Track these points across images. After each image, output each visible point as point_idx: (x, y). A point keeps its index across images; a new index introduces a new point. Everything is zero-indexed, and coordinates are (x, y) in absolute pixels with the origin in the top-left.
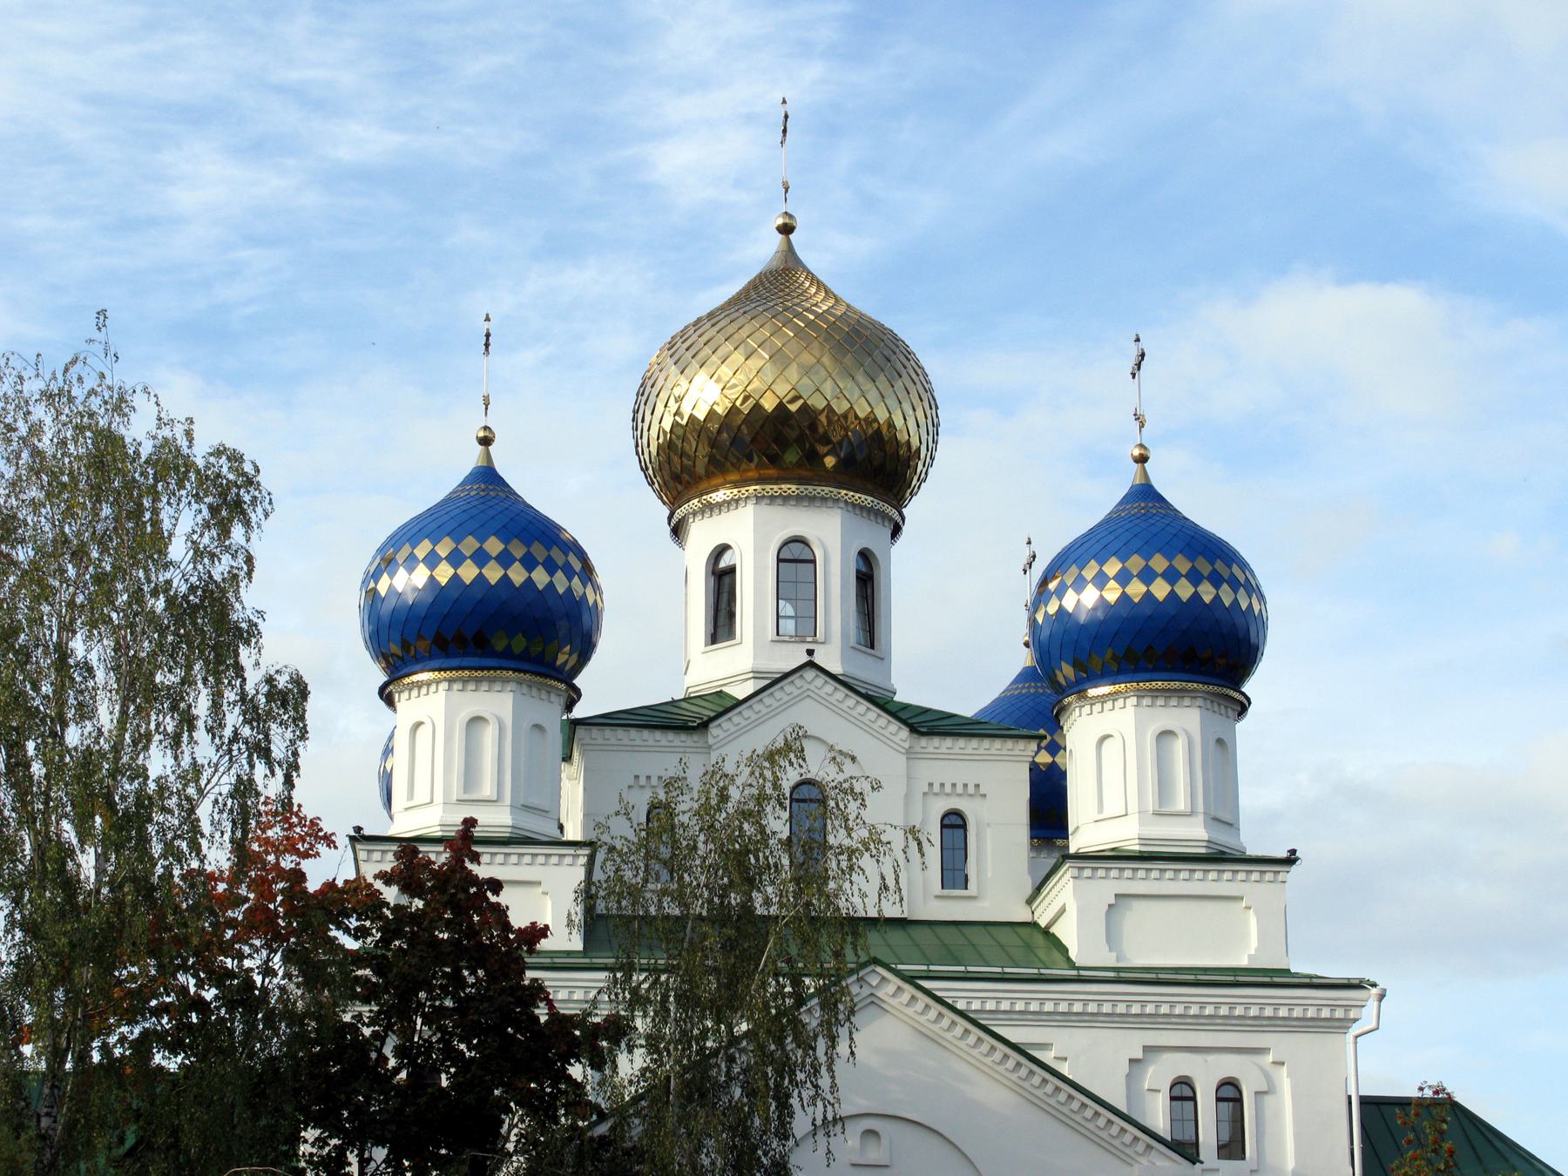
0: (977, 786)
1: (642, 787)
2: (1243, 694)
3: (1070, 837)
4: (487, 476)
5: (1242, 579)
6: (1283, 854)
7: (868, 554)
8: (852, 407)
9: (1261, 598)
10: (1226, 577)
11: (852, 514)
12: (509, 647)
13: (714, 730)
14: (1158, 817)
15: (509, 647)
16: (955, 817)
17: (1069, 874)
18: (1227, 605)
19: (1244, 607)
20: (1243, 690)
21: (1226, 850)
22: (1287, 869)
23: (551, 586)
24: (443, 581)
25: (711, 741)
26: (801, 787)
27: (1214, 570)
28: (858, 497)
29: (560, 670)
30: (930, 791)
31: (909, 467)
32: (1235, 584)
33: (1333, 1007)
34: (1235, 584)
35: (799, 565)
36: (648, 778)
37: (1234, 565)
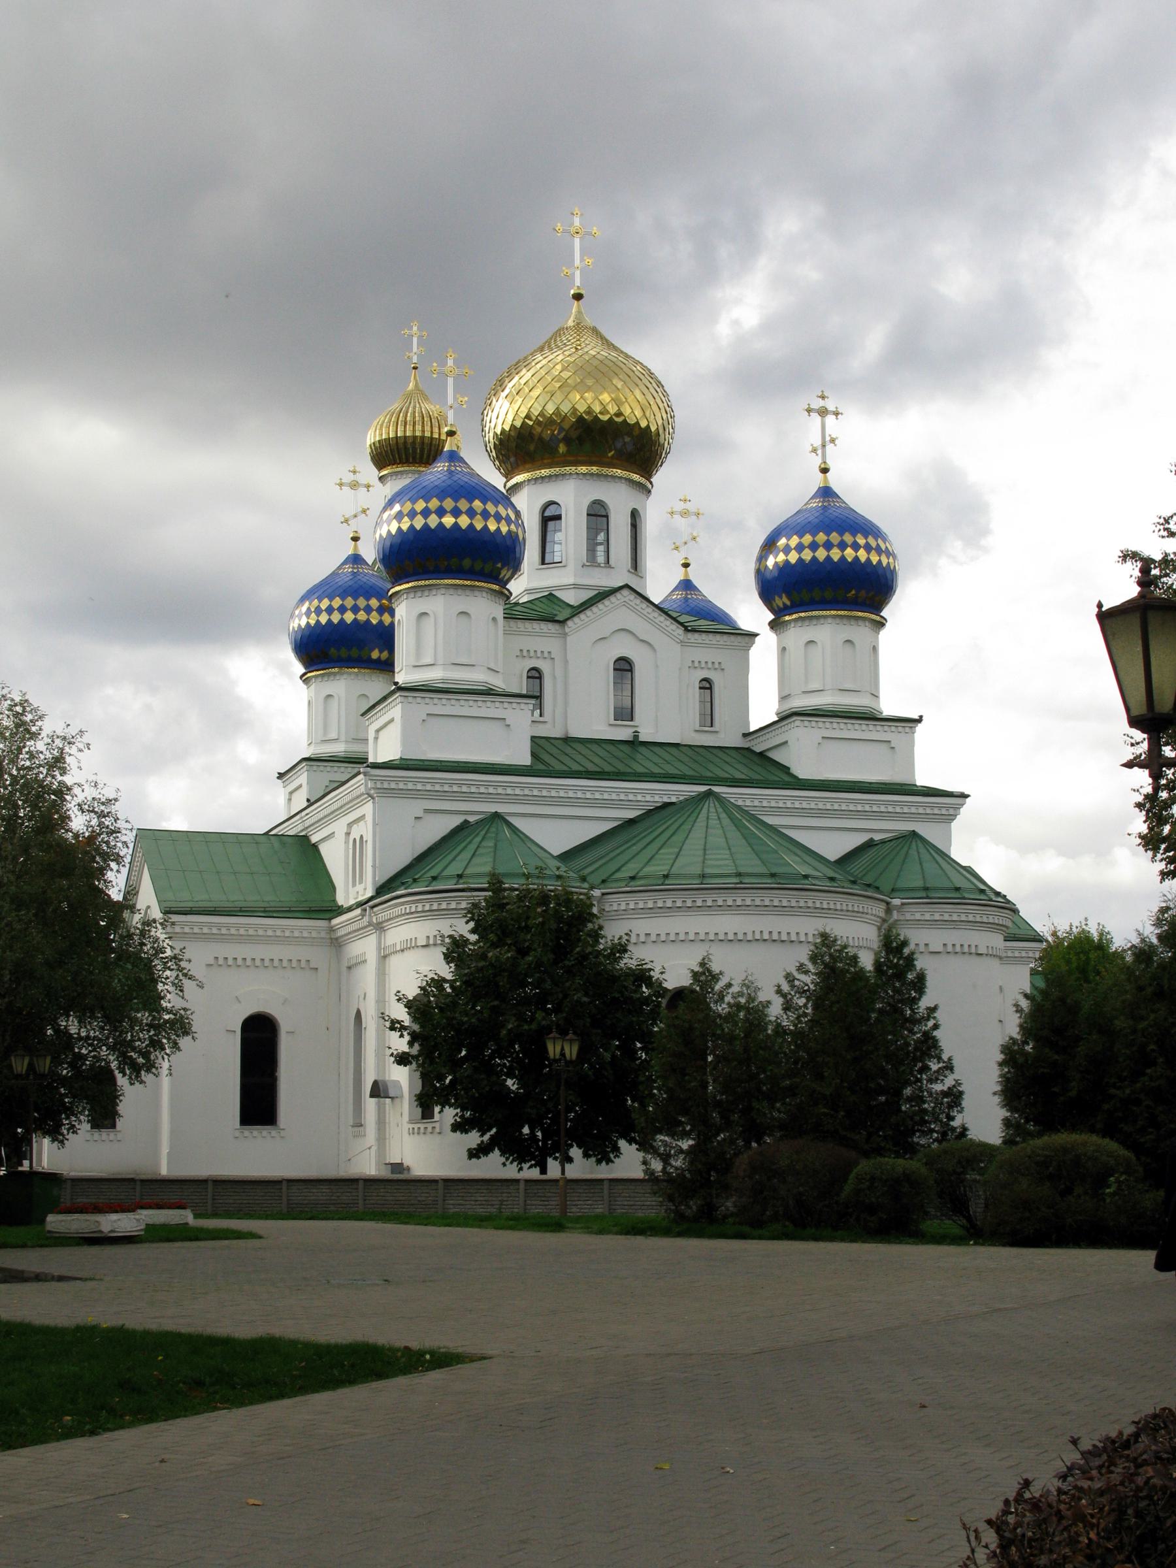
0: (720, 663)
1: (702, 668)
2: (508, 590)
3: (396, 675)
4: (826, 492)
5: (883, 548)
6: (916, 717)
7: (635, 514)
8: (633, 412)
9: (895, 557)
10: (874, 547)
11: (591, 481)
12: (483, 569)
13: (570, 623)
14: (490, 672)
15: (483, 569)
16: (535, 672)
17: (399, 700)
18: (874, 563)
19: (884, 564)
20: (882, 614)
21: (494, 688)
22: (780, 715)
23: (498, 529)
24: (464, 527)
25: (567, 630)
26: (622, 661)
27: (867, 542)
28: (583, 469)
29: (501, 581)
30: (522, 655)
31: (657, 454)
32: (879, 551)
33: (451, 785)
34: (879, 551)
35: (599, 518)
36: (706, 662)
37: (879, 539)
